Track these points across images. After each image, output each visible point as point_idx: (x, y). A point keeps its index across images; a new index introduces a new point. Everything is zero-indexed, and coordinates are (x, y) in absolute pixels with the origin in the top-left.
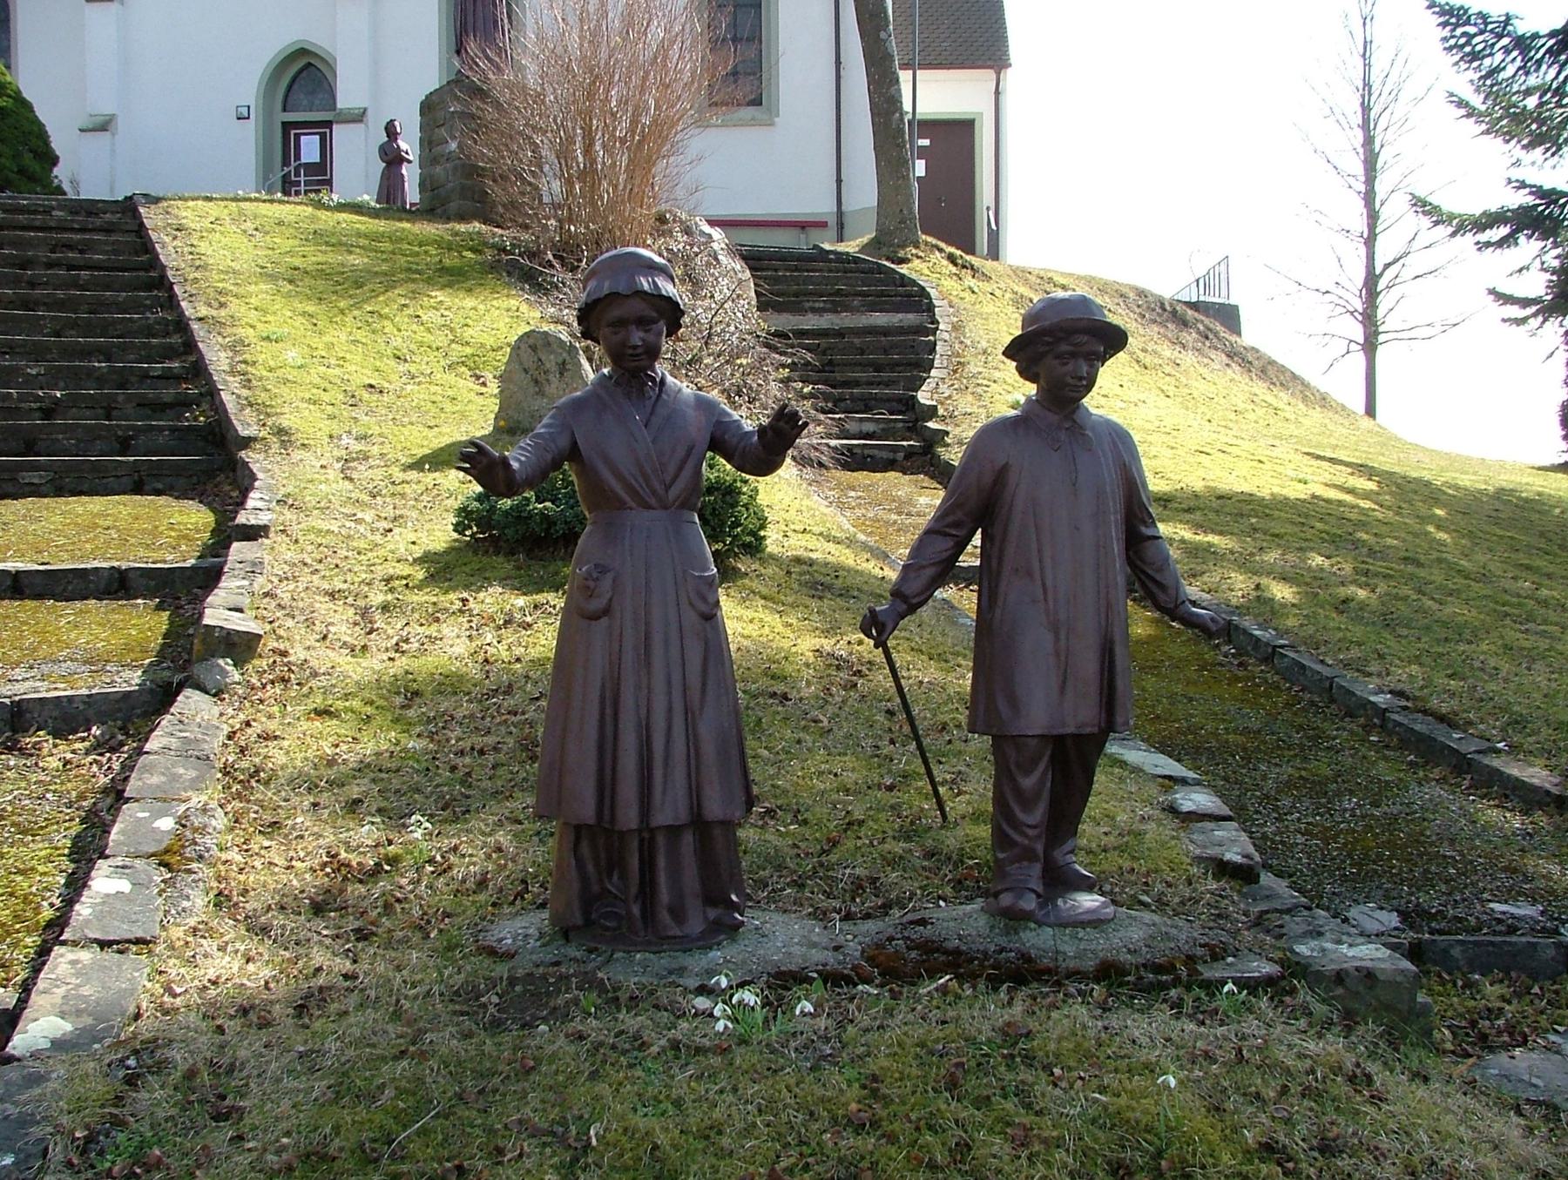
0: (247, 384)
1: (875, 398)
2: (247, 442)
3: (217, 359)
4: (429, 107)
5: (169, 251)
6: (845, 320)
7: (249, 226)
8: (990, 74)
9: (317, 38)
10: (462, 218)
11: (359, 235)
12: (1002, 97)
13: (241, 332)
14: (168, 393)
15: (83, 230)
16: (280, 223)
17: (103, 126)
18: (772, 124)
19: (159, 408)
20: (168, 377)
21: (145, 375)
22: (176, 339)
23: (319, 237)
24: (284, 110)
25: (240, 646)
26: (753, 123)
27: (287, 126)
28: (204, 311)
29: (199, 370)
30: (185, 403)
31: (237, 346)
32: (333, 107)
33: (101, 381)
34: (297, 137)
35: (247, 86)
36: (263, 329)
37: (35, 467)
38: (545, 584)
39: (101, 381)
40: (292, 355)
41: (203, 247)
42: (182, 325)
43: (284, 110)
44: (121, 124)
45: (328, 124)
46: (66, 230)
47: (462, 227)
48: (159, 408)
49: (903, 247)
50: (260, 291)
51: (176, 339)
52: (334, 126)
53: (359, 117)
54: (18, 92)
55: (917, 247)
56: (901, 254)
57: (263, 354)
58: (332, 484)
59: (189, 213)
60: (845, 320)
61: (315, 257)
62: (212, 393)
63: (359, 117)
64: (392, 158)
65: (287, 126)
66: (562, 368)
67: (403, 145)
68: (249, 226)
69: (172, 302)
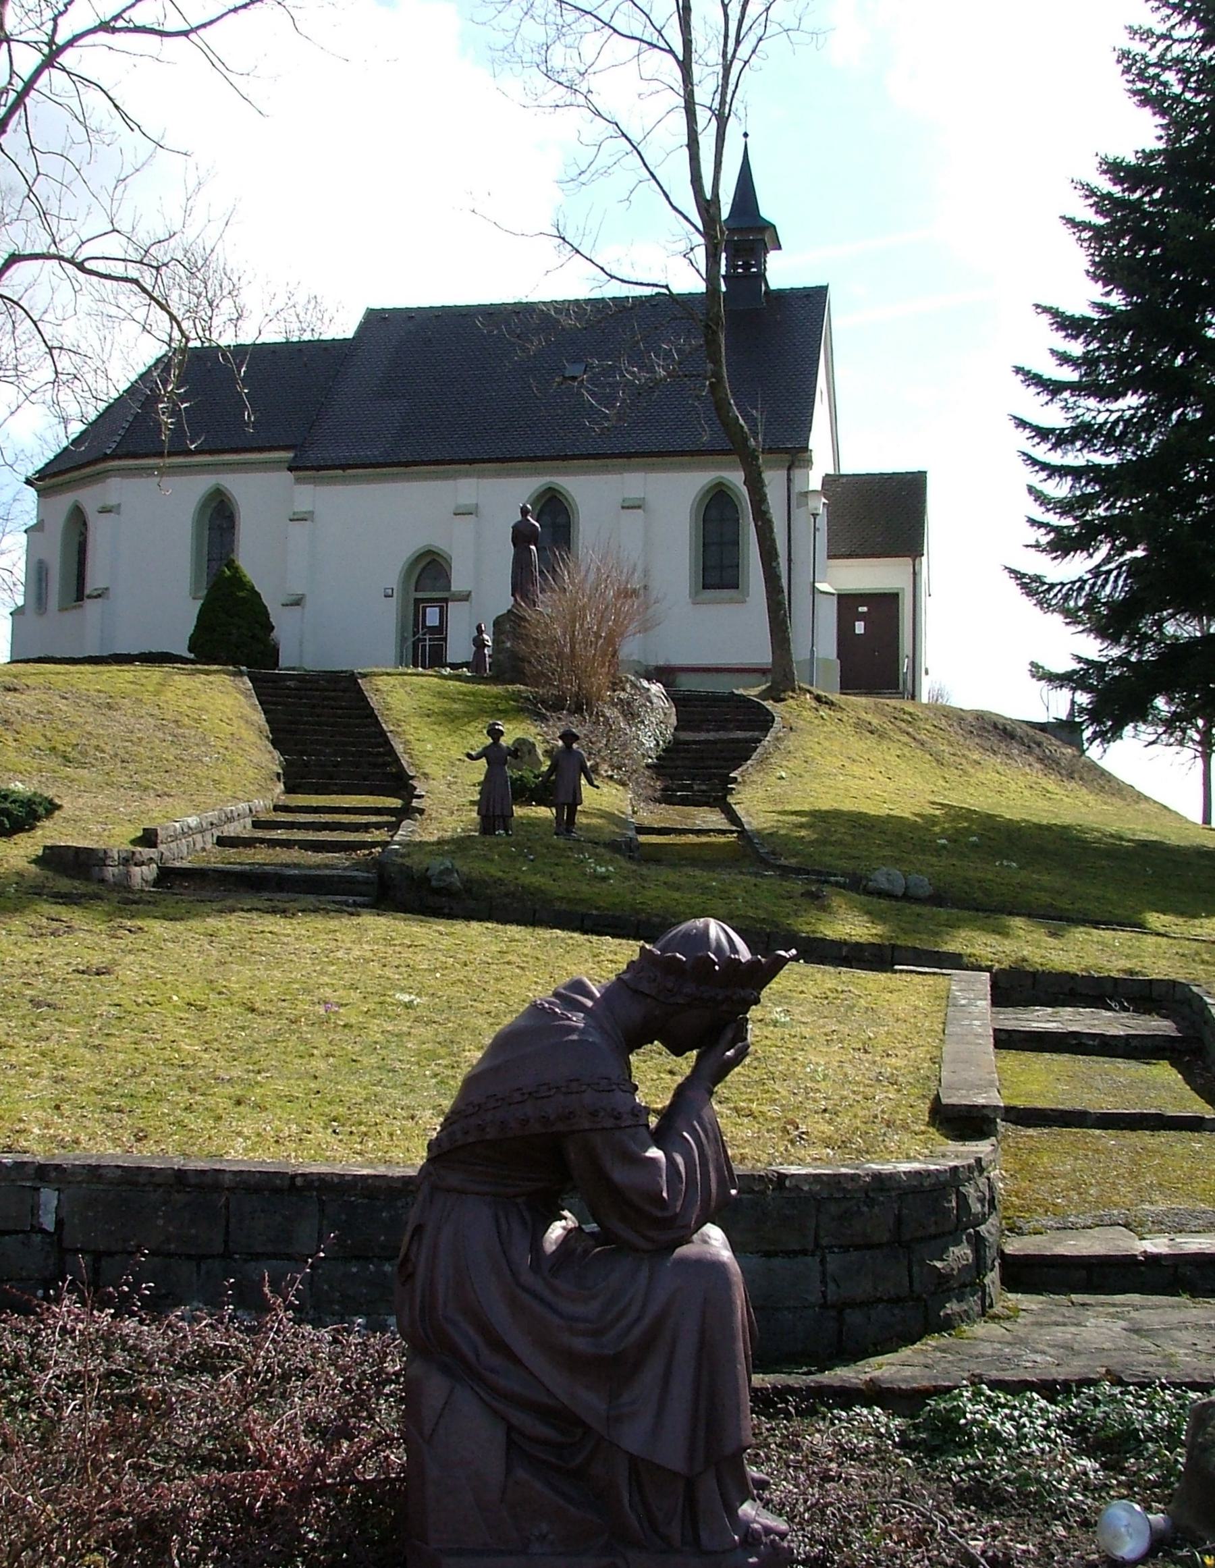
0: (411, 757)
1: (714, 774)
2: (412, 778)
3: (399, 748)
4: (497, 623)
5: (374, 701)
6: (722, 735)
7: (408, 689)
8: (909, 560)
9: (440, 544)
10: (512, 682)
11: (460, 693)
12: (918, 578)
13: (409, 737)
14: (380, 760)
15: (335, 691)
16: (422, 687)
17: (297, 602)
18: (744, 602)
19: (375, 765)
20: (379, 754)
21: (370, 753)
22: (381, 740)
23: (440, 695)
24: (416, 590)
25: (421, 811)
26: (731, 601)
27: (417, 601)
28: (392, 728)
29: (392, 751)
30: (386, 764)
31: (407, 742)
32: (448, 588)
33: (353, 755)
34: (424, 608)
35: (392, 575)
36: (417, 736)
37: (336, 784)
38: (866, 1189)
39: (353, 755)
40: (429, 747)
41: (389, 699)
42: (383, 733)
43: (416, 590)
44: (308, 602)
45: (446, 600)
46: (327, 690)
47: (510, 687)
48: (375, 765)
49: (784, 691)
50: (415, 721)
51: (381, 740)
52: (450, 604)
53: (466, 597)
54: (253, 587)
55: (793, 691)
56: (782, 696)
57: (417, 746)
58: (443, 788)
59: (380, 682)
60: (722, 735)
61: (439, 705)
62: (397, 760)
63: (466, 597)
64: (479, 644)
65: (417, 601)
66: (530, 752)
67: (486, 637)
68: (408, 689)
69: (378, 724)
